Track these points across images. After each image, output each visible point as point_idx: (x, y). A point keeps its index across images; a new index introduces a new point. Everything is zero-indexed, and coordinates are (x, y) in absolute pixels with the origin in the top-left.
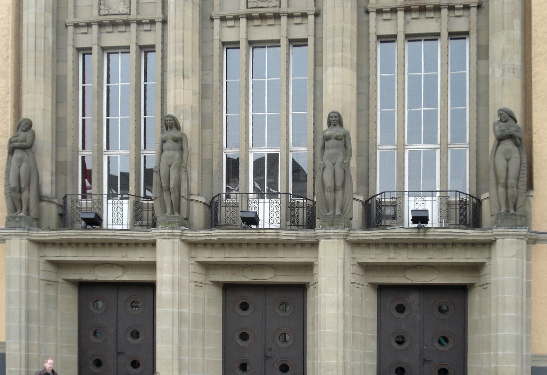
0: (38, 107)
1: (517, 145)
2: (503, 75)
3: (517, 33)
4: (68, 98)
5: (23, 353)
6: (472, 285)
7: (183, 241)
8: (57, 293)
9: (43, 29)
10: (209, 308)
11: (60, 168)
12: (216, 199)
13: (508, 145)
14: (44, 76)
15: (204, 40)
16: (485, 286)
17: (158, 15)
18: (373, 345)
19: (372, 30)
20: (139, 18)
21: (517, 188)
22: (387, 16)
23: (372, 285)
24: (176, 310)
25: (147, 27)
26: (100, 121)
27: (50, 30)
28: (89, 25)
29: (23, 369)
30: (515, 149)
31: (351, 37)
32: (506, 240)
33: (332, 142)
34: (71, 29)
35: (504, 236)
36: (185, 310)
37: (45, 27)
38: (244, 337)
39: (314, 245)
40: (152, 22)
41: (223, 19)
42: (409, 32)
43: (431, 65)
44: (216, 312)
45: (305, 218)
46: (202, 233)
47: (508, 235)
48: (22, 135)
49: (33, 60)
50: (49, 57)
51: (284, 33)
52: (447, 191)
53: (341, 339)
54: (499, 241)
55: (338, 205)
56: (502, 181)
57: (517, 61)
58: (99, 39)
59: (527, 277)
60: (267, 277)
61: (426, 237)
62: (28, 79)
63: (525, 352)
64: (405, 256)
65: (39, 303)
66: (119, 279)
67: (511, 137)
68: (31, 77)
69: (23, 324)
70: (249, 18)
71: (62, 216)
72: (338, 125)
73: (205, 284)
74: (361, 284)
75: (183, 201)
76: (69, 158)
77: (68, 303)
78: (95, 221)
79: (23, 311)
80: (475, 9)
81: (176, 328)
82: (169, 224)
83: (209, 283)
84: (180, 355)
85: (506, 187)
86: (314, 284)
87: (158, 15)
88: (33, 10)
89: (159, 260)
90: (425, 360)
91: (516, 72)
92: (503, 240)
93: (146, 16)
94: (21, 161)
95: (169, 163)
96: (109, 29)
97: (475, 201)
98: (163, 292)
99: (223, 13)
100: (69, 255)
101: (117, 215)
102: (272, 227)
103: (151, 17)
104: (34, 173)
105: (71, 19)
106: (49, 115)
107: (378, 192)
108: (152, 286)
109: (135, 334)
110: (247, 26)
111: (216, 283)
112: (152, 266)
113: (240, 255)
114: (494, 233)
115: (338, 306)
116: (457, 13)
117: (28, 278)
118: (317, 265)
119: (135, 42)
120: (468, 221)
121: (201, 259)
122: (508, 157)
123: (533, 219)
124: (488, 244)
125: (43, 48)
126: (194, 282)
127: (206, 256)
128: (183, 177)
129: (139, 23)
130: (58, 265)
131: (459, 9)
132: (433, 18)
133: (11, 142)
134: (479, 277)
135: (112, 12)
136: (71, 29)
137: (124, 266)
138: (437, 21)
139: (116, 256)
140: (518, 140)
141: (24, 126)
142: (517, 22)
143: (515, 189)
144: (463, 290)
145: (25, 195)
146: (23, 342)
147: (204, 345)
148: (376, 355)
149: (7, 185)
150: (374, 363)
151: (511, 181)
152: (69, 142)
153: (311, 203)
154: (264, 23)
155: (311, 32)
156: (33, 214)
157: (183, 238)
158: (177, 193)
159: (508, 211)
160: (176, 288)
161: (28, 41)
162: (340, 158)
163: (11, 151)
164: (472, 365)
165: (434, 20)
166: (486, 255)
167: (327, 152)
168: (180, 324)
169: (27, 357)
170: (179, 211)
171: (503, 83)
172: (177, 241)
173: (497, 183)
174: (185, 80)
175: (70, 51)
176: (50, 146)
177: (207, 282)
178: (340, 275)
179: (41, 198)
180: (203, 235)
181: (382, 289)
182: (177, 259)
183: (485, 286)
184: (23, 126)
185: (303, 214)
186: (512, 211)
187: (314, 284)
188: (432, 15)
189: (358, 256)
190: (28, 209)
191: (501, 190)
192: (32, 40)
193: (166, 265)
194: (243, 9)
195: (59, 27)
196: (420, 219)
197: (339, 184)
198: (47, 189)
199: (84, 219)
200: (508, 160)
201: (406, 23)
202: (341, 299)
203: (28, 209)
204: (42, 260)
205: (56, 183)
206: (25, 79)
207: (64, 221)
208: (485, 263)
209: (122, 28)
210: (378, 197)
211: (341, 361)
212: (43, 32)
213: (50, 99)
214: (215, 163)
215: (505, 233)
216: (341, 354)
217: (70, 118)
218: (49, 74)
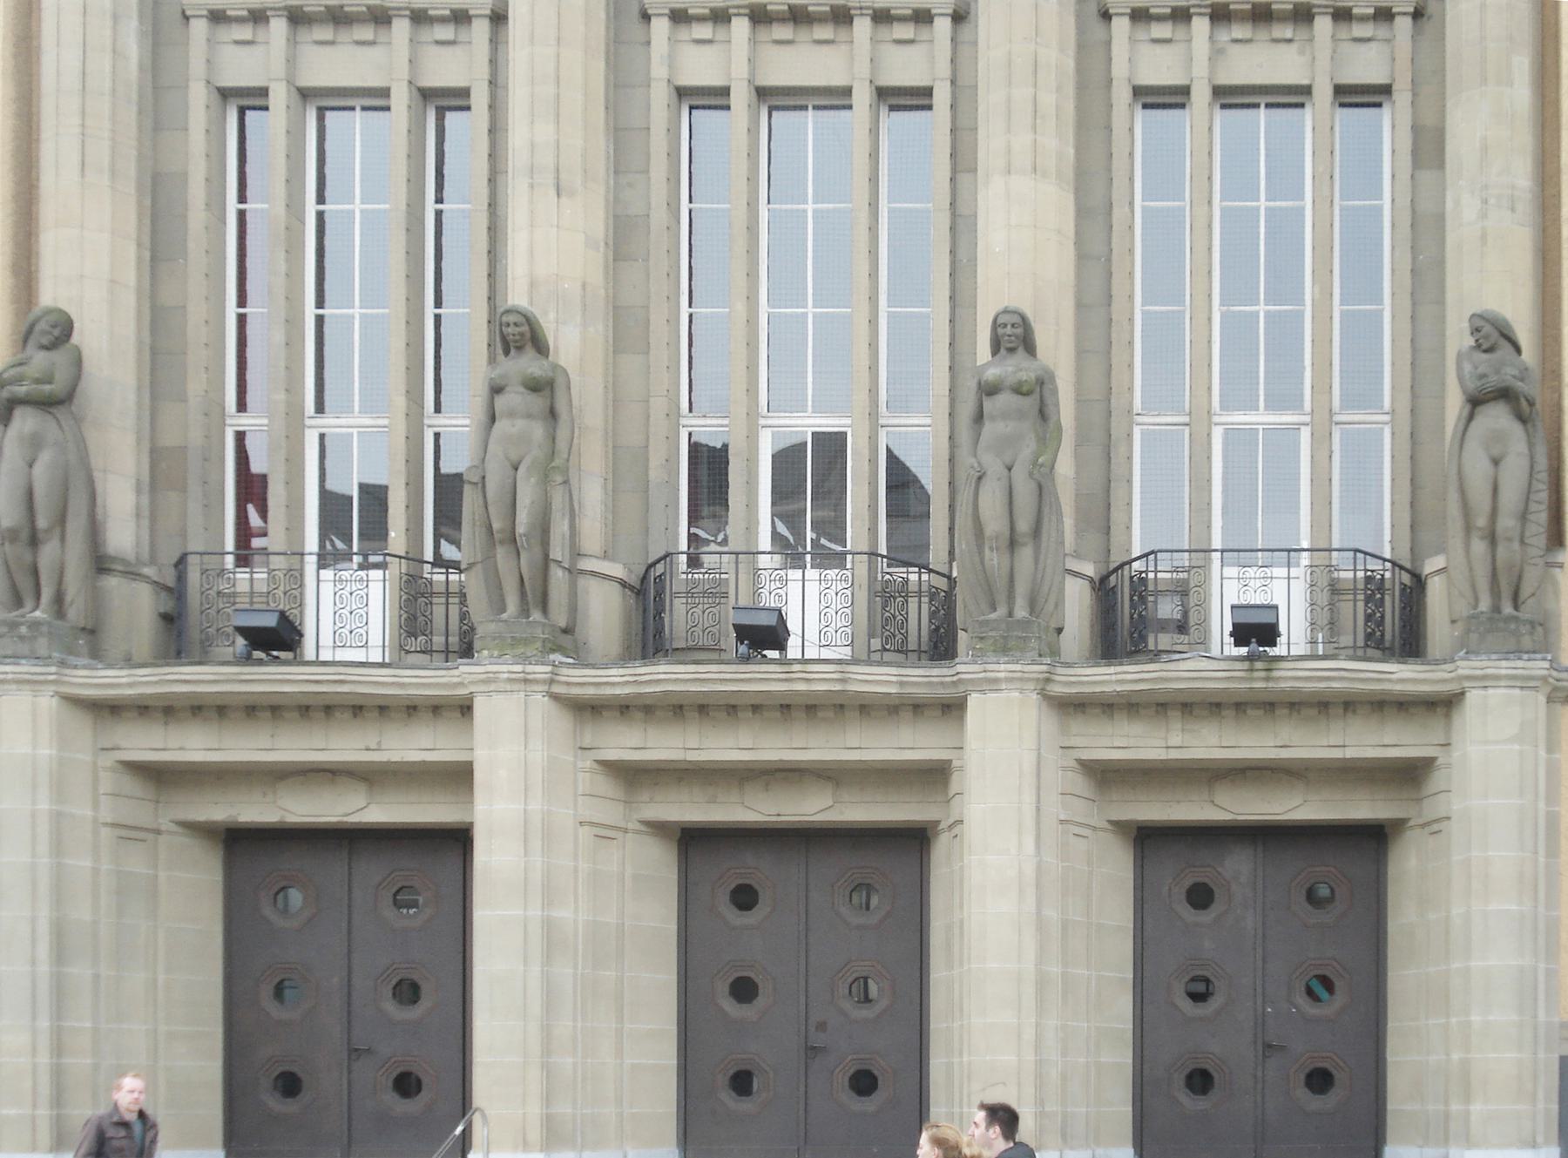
1: (1522, 419)
2: (1483, 215)
3: (1522, 95)
4: (191, 245)
5: (44, 1059)
6: (1399, 825)
7: (555, 697)
9: (109, 23)
10: (640, 903)
11: (163, 471)
12: (660, 568)
13: (1497, 417)
14: (113, 173)
15: (621, 81)
16: (1435, 826)
18: (1123, 1005)
19: (1120, 69)
22: (1162, 30)
23: (1119, 826)
24: (535, 912)
26: (293, 322)
30: (1517, 429)
32: (1491, 691)
33: (1004, 400)
36: (563, 913)
37: (116, 18)
38: (744, 990)
39: (952, 709)
42: (1224, 79)
43: (1285, 181)
47: (1497, 678)
48: (40, 360)
49: (76, 120)
50: (130, 115)
51: (863, 70)
52: (1330, 550)
54: (1473, 697)
55: (1021, 589)
56: (1481, 521)
57: (1522, 176)
58: (291, 61)
64: (1214, 741)
67: (1505, 394)
69: (44, 968)
71: (172, 621)
72: (1021, 350)
73: (626, 831)
75: (558, 575)
76: (196, 437)
77: (193, 892)
79: (44, 927)
80: (1408, 21)
82: (512, 644)
83: (639, 826)
84: (547, 1050)
85: (1492, 538)
86: (950, 827)
92: (1482, 692)
95: (514, 457)
96: (782, 31)
97: (1406, 578)
98: (495, 860)
100: (194, 745)
101: (349, 618)
102: (341, 655)
106: (129, 300)
107: (1136, 553)
110: (753, 41)
111: (659, 828)
112: (459, 777)
113: (730, 742)
114: (1460, 672)
116: (1359, 30)
117: (58, 818)
118: (1449, 766)
119: (1205, 73)
120: (1388, 637)
121: (612, 755)
122: (1496, 452)
124: (1443, 705)
125: (108, 84)
126: (592, 824)
131: (1363, 19)
132: (1290, 41)
134: (1419, 800)
137: (371, 777)
138: (1301, 52)
140: (1524, 403)
142: (1522, 65)
144: (1374, 838)
146: (44, 1023)
151: (1507, 523)
152: (196, 386)
153: (942, 583)
154: (804, 34)
155: (944, 69)
157: (556, 689)
158: (537, 550)
159: (1496, 609)
160: (536, 844)
162: (1028, 449)
165: (1294, 47)
167: (989, 428)
169: (58, 1073)
171: (1484, 237)
172: (540, 701)
173: (1468, 528)
174: (564, 199)
175: (198, 97)
176: (132, 397)
177: (630, 826)
179: (101, 564)
180: (621, 680)
181: (692, 842)
182: (538, 755)
183: (1435, 827)
184: (44, 333)
185: (918, 617)
186: (1508, 609)
187: (950, 827)
188: (1288, 34)
190: (59, 600)
191: (1479, 547)
196: (1256, 632)
197: (1023, 526)
198: (122, 537)
199: (244, 631)
200: (1496, 462)
201: (1217, 53)
203: (59, 600)
205: (152, 515)
207: (177, 634)
208: (1433, 760)
209: (366, 32)
210: (1136, 565)
211: (1029, 1057)
212: (108, 32)
213: (131, 250)
215: (1489, 671)
216: (1029, 1034)
217: (197, 312)
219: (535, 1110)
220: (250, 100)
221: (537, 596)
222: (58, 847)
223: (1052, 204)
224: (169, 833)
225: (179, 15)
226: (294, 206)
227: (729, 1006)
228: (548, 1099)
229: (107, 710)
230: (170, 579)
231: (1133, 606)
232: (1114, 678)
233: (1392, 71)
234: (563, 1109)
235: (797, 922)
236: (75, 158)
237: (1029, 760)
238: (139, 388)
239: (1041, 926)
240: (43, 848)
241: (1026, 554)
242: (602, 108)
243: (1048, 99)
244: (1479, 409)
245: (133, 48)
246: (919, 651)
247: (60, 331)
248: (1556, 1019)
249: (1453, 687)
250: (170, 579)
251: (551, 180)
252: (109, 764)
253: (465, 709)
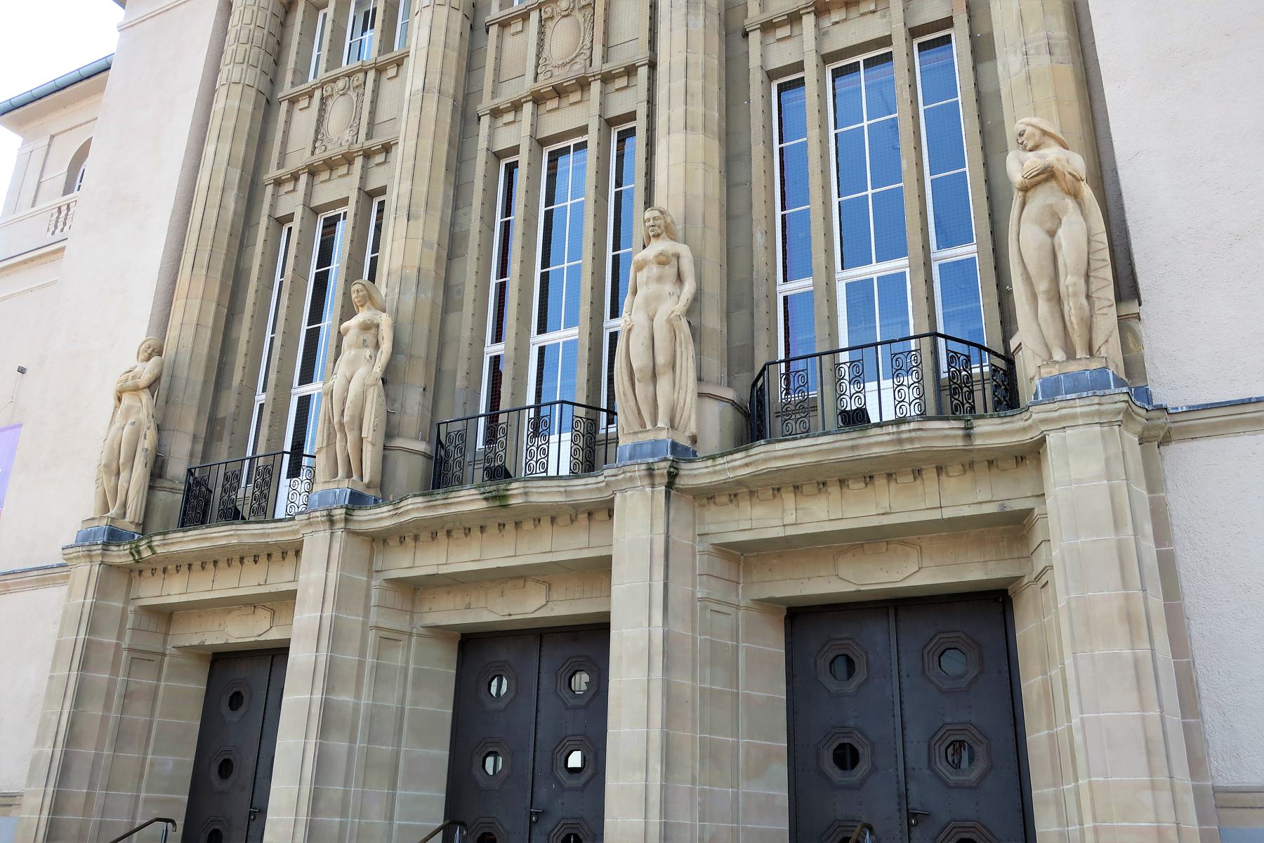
8: (159, 680)
16: (1042, 579)
19: (755, 61)
22: (784, 32)
26: (290, 335)
31: (705, 77)
32: (1069, 431)
35: (1063, 423)
36: (344, 698)
42: (829, 48)
43: (883, 103)
47: (1074, 417)
54: (1051, 440)
59: (1156, 539)
60: (530, 606)
61: (856, 453)
66: (262, 638)
69: (656, 733)
72: (664, 235)
74: (729, 604)
81: (312, 741)
83: (422, 631)
85: (1057, 298)
86: (1038, 578)
90: (911, 815)
91: (1057, 51)
96: (552, 104)
110: (603, 93)
125: (214, 223)
134: (1029, 558)
147: (393, 786)
151: (1070, 281)
158: (356, 433)
160: (324, 642)
164: (1045, 823)
166: (1028, 488)
168: (324, 731)
181: (800, 618)
183: (1043, 581)
187: (1038, 578)
189: (713, 528)
191: (1044, 307)
193: (311, 590)
203: (125, 505)
208: (1032, 510)
211: (655, 820)
212: (219, 198)
217: (759, 209)
218: (219, 265)
223: (707, 150)
224: (171, 656)
225: (740, 34)
226: (300, 272)
231: (224, 490)
232: (726, 466)
233: (1154, 482)
235: (520, 697)
238: (205, 382)
242: (443, 170)
243: (696, 84)
244: (1029, 194)
245: (231, 204)
249: (1034, 434)
251: (406, 213)
252: (378, 582)
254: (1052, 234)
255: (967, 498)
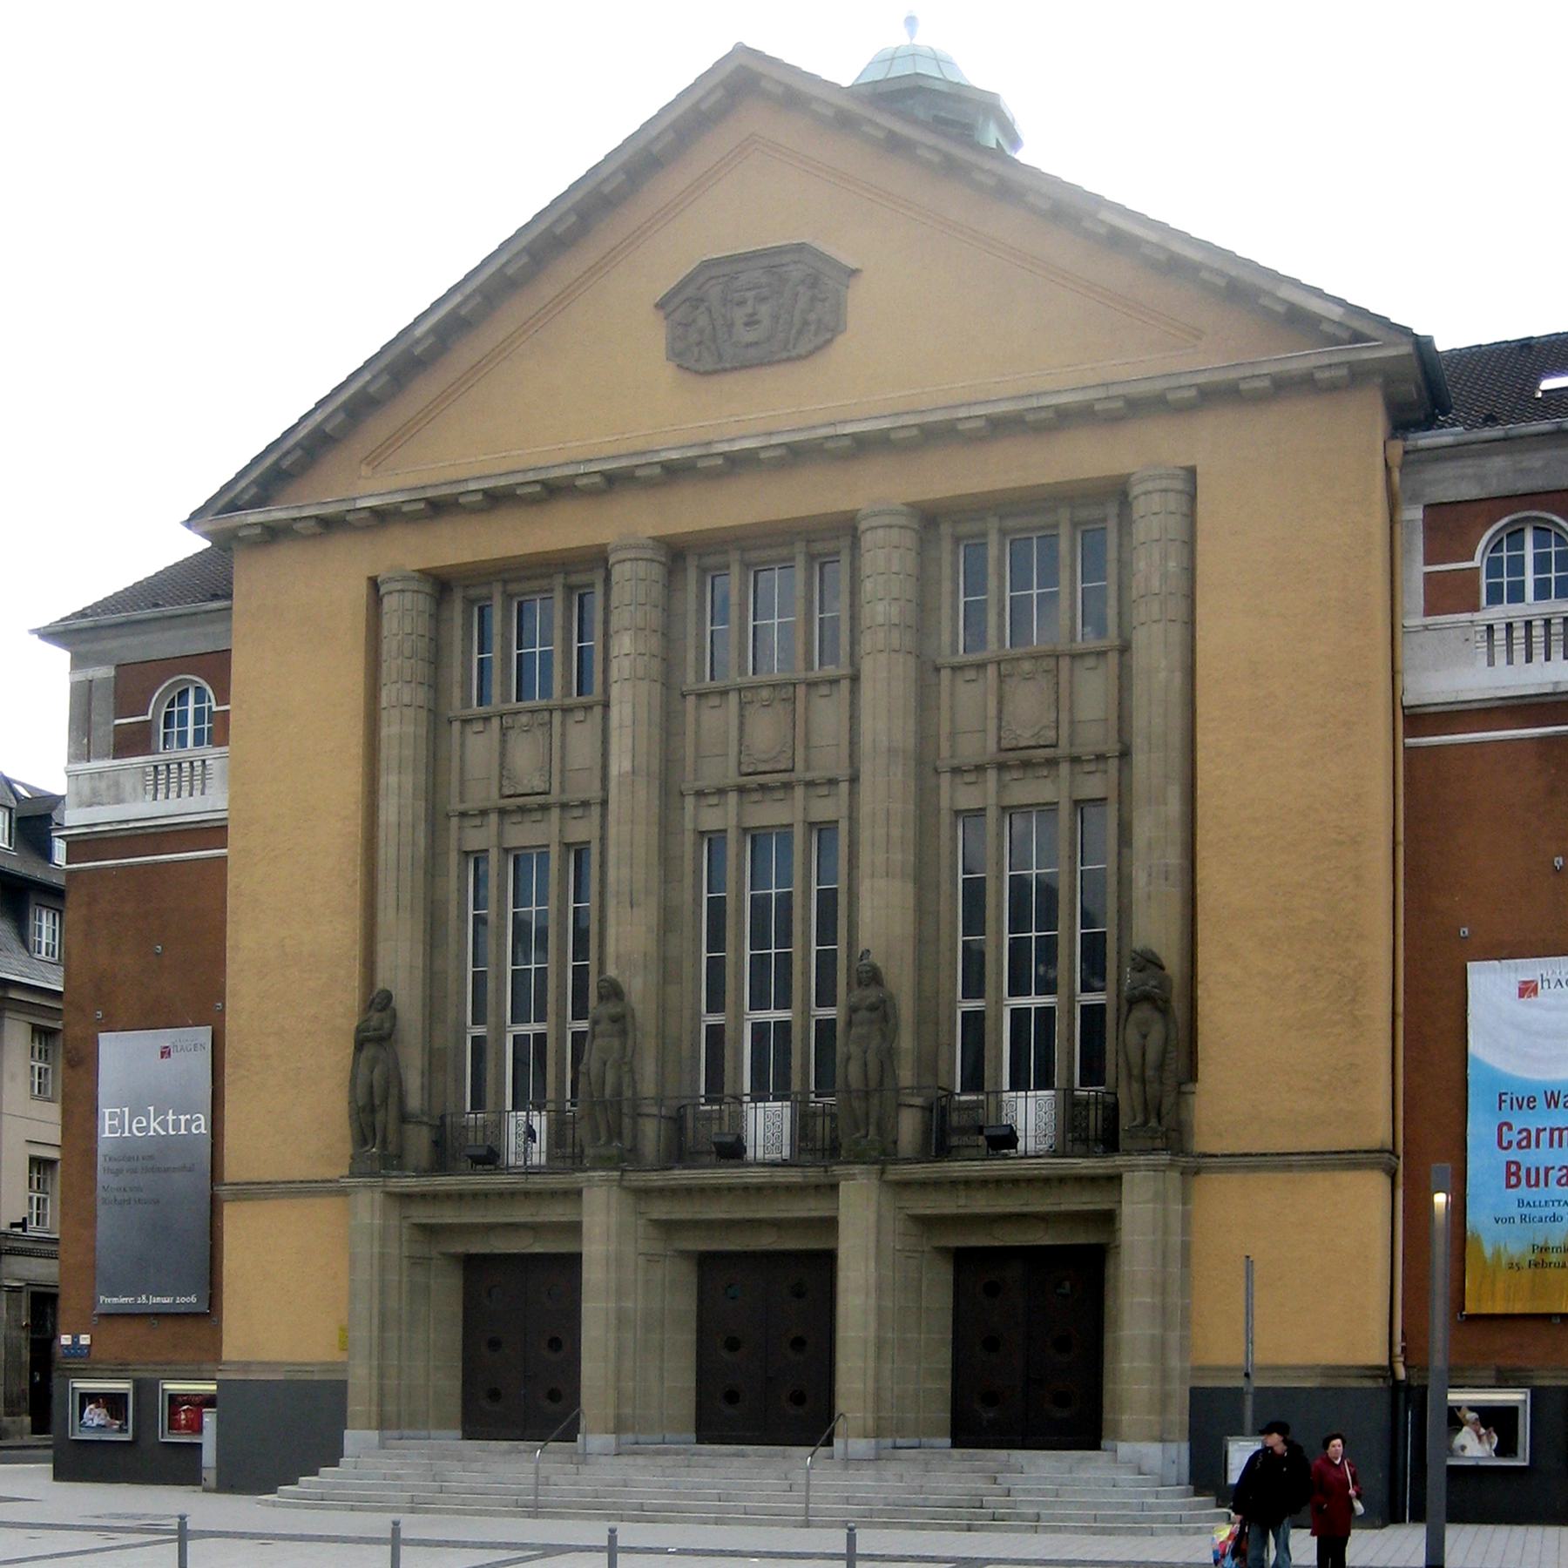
0: (400, 968)
1: (1158, 1009)
2: (1149, 883)
11: (436, 1060)
13: (1143, 1012)
14: (412, 910)
17: (594, 793)
18: (946, 1354)
19: (945, 803)
20: (565, 798)
21: (1161, 1082)
23: (942, 1251)
24: (612, 1305)
25: (577, 812)
27: (422, 826)
28: (484, 813)
29: (374, 1408)
30: (1157, 1016)
33: (863, 1015)
34: (455, 821)
35: (1133, 1168)
36: (629, 1304)
38: (494, 1344)
40: (585, 804)
41: (700, 794)
42: (1007, 802)
44: (686, 1303)
45: (819, 1145)
46: (654, 1176)
48: (376, 1018)
50: (420, 875)
53: (871, 1350)
55: (873, 1120)
56: (1136, 1072)
58: (500, 834)
62: (387, 915)
63: (1175, 1362)
64: (983, 1202)
65: (400, 1299)
67: (1147, 998)
68: (391, 912)
69: (375, 1333)
70: (1002, 767)
71: (438, 1144)
75: (626, 1121)
77: (447, 1290)
78: (490, 1158)
79: (375, 1311)
82: (603, 1163)
84: (618, 1380)
85: (1143, 1081)
87: (594, 793)
88: (394, 800)
89: (586, 1220)
91: (1171, 877)
93: (574, 796)
94: (373, 1063)
96: (756, 796)
98: (593, 1275)
99: (700, 785)
100: (448, 1216)
101: (525, 1135)
103: (830, 775)
104: (394, 1079)
105: (456, 806)
108: (575, 1260)
109: (798, 1344)
111: (684, 1254)
112: (575, 1229)
115: (867, 1295)
116: (1088, 768)
117: (382, 1255)
121: (655, 1216)
123: (1196, 1130)
127: (662, 1210)
128: (626, 1080)
129: (564, 806)
130: (430, 1231)
133: (359, 1030)
135: (520, 790)
136: (455, 821)
137: (535, 1229)
139: (521, 1214)
140: (1160, 1003)
141: (378, 1003)
143: (1156, 1086)
145: (380, 1117)
148: (949, 1372)
149: (353, 1100)
150: (946, 1385)
151: (1150, 1073)
152: (451, 1015)
155: (844, 811)
156: (391, 1148)
159: (1146, 1122)
161: (387, 853)
162: (875, 1042)
163: (360, 1045)
169: (381, 1389)
170: (620, 1136)
173: (1130, 1076)
175: (454, 858)
178: (872, 1237)
179: (404, 1118)
180: (656, 1179)
181: (963, 1259)
186: (1153, 1123)
190: (384, 1141)
191: (1136, 1086)
192: (392, 852)
194: (733, 778)
195: (435, 818)
197: (873, 1084)
198: (414, 1102)
199: (470, 1157)
201: (1002, 787)
202: (872, 1281)
203: (384, 1141)
204: (405, 1224)
205: (428, 1089)
206: (381, 917)
207: (441, 1162)
209: (538, 816)
213: (420, 947)
214: (686, 1044)
216: (871, 1372)
219: (611, 1412)
220: (479, 857)
221: (616, 1133)
222: (383, 1270)
227: (725, 1354)
228: (618, 1406)
229: (406, 1198)
230: (438, 1123)
234: (628, 1411)
236: (394, 904)
237: (872, 1218)
239: (880, 1312)
240: (375, 1327)
241: (875, 1101)
245: (422, 842)
246: (824, 1150)
247: (387, 997)
248: (1188, 1365)
250: (438, 1123)
253: (579, 1193)
254: (1145, 1036)
255: (555, 1213)
